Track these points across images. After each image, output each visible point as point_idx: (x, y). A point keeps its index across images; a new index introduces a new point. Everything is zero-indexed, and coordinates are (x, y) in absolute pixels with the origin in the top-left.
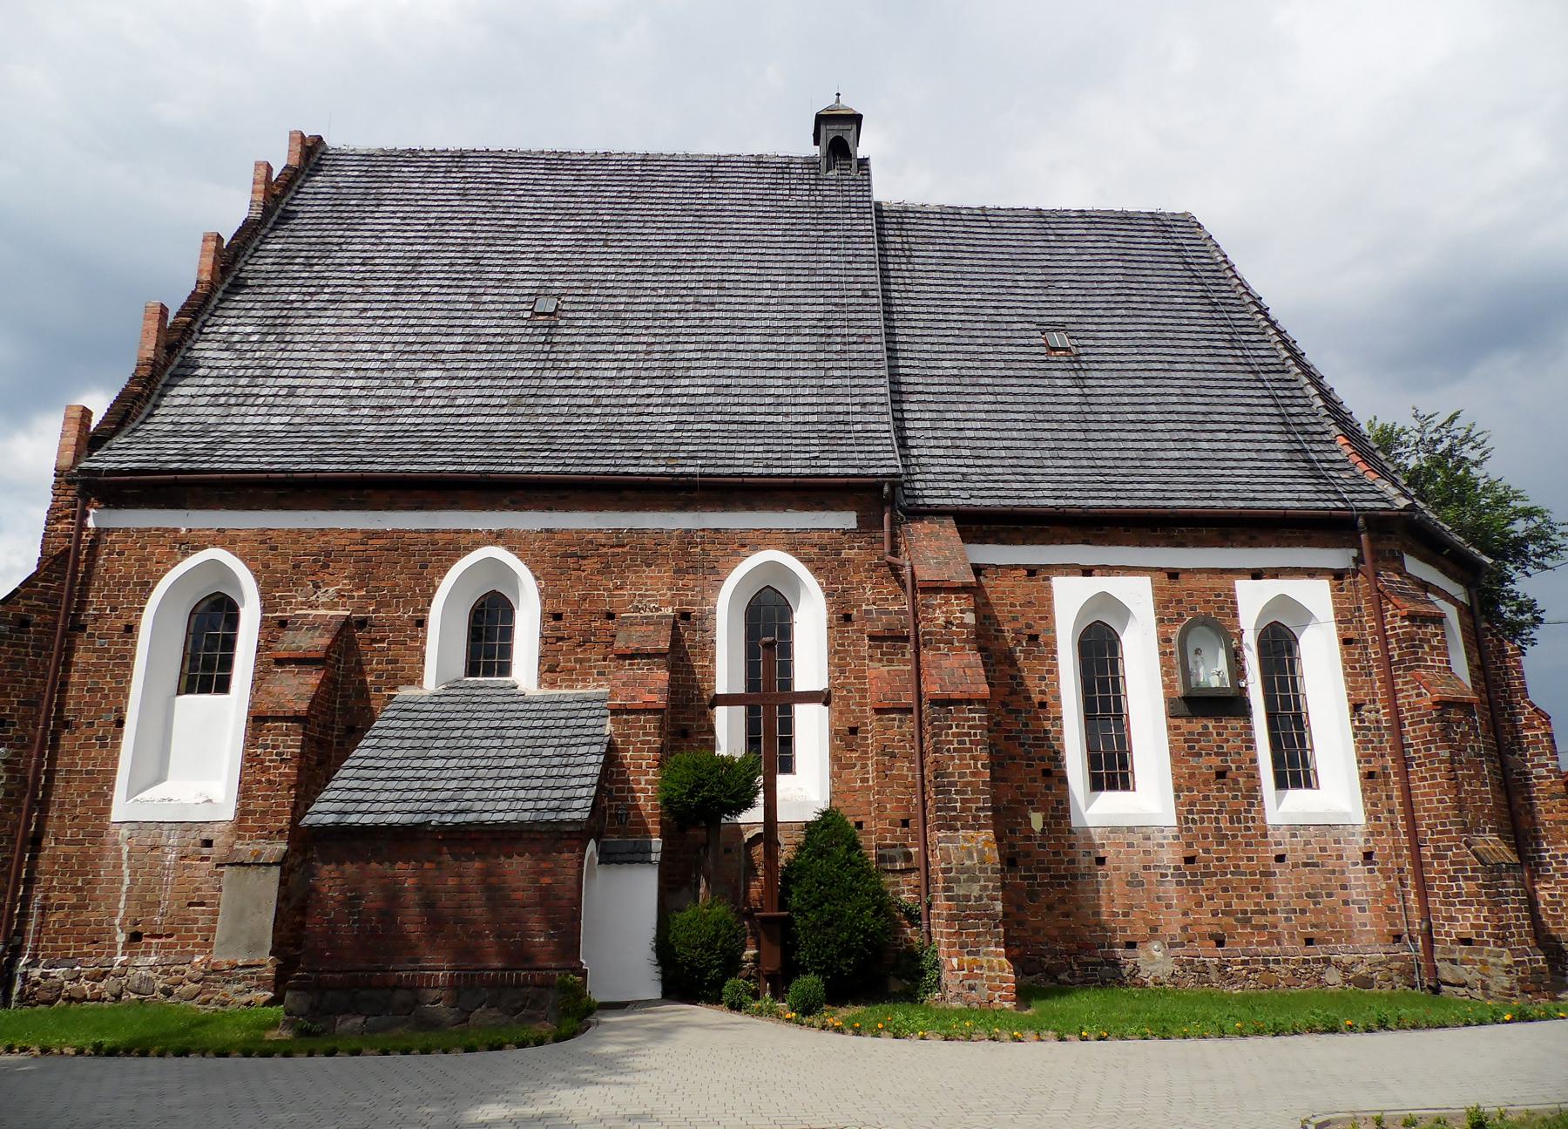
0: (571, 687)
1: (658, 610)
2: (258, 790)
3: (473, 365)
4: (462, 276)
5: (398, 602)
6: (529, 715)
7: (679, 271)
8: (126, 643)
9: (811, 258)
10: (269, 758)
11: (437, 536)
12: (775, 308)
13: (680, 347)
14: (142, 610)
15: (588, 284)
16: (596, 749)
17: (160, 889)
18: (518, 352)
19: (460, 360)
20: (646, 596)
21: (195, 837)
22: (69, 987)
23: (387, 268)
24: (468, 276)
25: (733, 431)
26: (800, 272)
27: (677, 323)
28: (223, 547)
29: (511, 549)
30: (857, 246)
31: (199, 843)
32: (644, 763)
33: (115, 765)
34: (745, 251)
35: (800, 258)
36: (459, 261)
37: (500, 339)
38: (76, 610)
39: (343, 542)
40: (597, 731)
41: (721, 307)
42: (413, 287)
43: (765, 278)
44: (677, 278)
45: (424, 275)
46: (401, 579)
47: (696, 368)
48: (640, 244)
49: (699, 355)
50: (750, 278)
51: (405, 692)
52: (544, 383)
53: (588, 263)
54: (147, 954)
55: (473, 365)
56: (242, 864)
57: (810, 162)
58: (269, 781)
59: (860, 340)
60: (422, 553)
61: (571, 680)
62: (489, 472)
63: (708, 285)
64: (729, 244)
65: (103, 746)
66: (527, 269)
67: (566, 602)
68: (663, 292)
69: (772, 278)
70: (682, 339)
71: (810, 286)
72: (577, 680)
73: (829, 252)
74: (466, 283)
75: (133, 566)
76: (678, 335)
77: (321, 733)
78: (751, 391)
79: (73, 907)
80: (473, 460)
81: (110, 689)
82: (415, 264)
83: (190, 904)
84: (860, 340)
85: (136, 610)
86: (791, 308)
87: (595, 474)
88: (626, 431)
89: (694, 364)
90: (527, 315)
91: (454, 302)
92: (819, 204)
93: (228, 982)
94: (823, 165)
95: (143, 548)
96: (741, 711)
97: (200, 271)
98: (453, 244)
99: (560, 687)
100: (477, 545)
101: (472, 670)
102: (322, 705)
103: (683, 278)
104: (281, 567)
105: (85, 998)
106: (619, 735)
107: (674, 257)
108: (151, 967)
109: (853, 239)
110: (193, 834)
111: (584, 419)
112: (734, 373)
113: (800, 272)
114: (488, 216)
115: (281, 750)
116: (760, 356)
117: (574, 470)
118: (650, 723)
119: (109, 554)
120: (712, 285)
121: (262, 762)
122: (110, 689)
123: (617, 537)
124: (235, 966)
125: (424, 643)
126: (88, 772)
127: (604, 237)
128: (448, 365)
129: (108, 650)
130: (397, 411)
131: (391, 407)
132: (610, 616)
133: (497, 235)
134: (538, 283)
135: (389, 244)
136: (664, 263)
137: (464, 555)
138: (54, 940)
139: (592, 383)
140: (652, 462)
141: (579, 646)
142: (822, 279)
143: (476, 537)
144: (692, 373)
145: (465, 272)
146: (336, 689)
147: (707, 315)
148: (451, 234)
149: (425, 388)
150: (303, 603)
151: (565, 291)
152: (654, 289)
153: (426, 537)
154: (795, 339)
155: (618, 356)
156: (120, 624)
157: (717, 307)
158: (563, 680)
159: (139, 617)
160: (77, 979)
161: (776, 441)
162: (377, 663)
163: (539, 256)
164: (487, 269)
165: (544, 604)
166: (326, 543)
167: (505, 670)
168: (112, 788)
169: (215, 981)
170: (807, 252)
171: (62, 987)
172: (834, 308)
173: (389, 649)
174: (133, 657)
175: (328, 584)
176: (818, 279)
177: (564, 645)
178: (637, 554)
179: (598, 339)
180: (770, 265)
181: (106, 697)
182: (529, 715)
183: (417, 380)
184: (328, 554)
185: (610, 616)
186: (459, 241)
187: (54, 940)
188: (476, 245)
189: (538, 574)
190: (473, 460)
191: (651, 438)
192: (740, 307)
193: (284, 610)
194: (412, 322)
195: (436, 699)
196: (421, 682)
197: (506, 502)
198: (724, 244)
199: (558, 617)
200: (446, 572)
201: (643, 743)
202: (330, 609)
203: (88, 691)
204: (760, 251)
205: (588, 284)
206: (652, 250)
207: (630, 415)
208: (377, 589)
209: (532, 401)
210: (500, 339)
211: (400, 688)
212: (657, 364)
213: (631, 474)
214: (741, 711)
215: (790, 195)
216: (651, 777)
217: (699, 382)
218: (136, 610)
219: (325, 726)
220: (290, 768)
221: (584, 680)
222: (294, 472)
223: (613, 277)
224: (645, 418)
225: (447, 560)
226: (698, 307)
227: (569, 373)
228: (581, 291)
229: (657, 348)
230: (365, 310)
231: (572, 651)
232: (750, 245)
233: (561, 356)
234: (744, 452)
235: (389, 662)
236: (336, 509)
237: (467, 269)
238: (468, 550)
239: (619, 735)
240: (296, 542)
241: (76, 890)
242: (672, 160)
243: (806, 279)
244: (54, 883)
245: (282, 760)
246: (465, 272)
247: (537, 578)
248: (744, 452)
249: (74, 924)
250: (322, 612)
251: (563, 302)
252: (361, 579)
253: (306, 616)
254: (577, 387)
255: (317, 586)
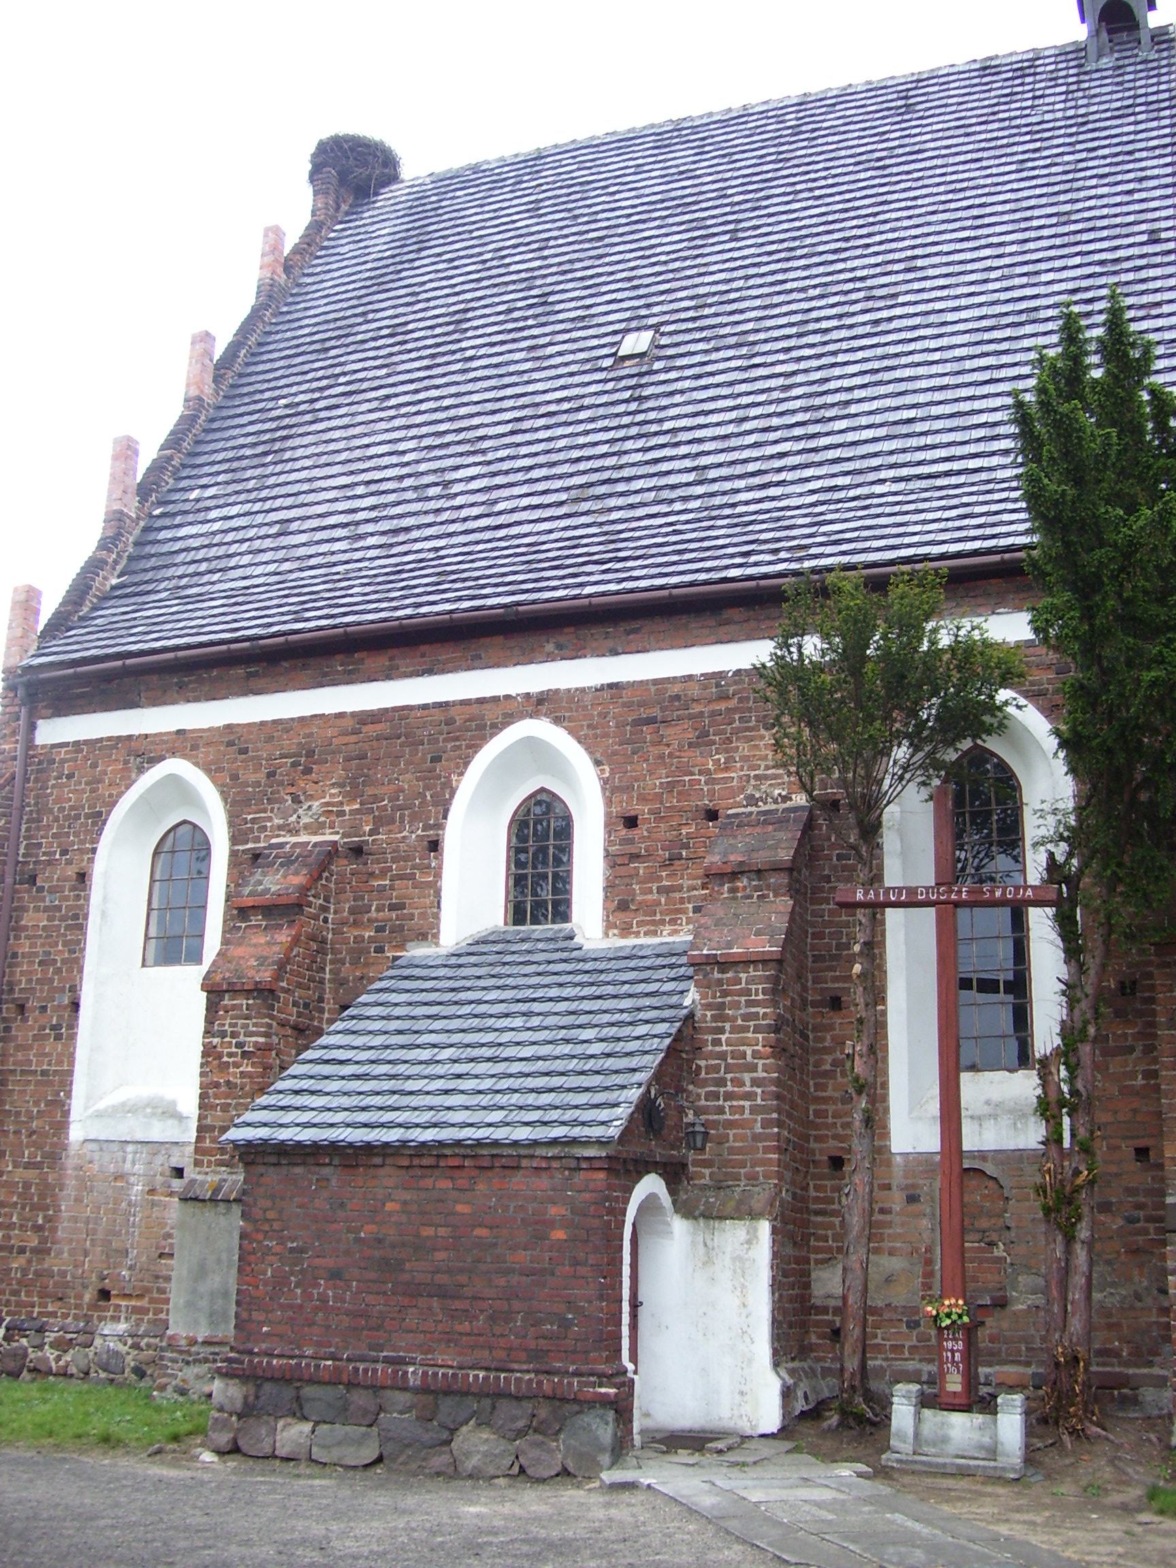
0: (655, 933)
1: (786, 799)
2: (216, 1096)
3: (524, 450)
4: (521, 324)
5: (402, 817)
6: (578, 978)
7: (843, 255)
8: (78, 897)
9: (1062, 198)
10: (228, 1048)
11: (452, 712)
12: (997, 285)
13: (837, 371)
14: (94, 851)
15: (700, 302)
16: (661, 1028)
17: (127, 1233)
18: (592, 420)
19: (507, 446)
20: (766, 777)
21: (162, 1163)
22: (32, 1356)
23: (422, 333)
24: (530, 322)
25: (912, 492)
26: (1042, 222)
27: (835, 335)
28: (184, 757)
29: (557, 721)
30: (1143, 164)
31: (168, 1173)
32: (749, 1053)
33: (72, 1063)
34: (953, 205)
35: (1044, 201)
36: (520, 304)
37: (566, 406)
38: (24, 855)
39: (330, 733)
40: (674, 1000)
41: (907, 298)
42: (454, 352)
43: (983, 242)
44: (840, 266)
45: (470, 334)
46: (407, 781)
47: (860, 401)
48: (786, 226)
49: (867, 379)
50: (959, 246)
51: (418, 951)
52: (625, 459)
53: (703, 270)
54: (116, 1319)
55: (524, 450)
56: (196, 1199)
57: (1075, 53)
58: (228, 1083)
59: (1141, 313)
60: (433, 741)
61: (653, 923)
62: (518, 604)
63: (889, 268)
64: (927, 201)
65: (58, 1037)
66: (614, 296)
67: (643, 799)
68: (817, 292)
69: (995, 240)
70: (841, 358)
71: (1058, 241)
72: (662, 922)
73: (1094, 182)
74: (526, 333)
75: (84, 791)
76: (834, 353)
77: (299, 1015)
78: (949, 423)
79: (35, 1251)
80: (501, 589)
81: (64, 961)
82: (459, 321)
83: (161, 1256)
84: (1141, 313)
85: (87, 851)
86: (1024, 280)
87: (676, 586)
88: (740, 515)
89: (858, 394)
90: (608, 362)
91: (714, 327)
92: (1082, 111)
93: (188, 1363)
94: (1092, 50)
95: (94, 766)
96: (928, 915)
97: (188, 385)
98: (514, 282)
99: (637, 934)
100: (509, 719)
101: (518, 914)
102: (299, 975)
103: (849, 264)
104: (252, 778)
105: (50, 1372)
106: (708, 1006)
107: (836, 236)
108: (120, 1338)
109: (1137, 155)
110: (160, 1159)
111: (678, 506)
112: (922, 398)
113: (1042, 222)
114: (565, 232)
115: (242, 1038)
116: (968, 364)
117: (643, 584)
118: (754, 982)
119: (57, 778)
120: (896, 267)
121: (220, 1056)
122: (64, 961)
123: (718, 685)
124: (192, 1342)
125: (438, 875)
126: (44, 1073)
127: (731, 227)
128: (490, 456)
129: (59, 908)
130: (415, 534)
131: (407, 530)
132: (712, 815)
133: (576, 256)
134: (627, 315)
135: (428, 300)
136: (821, 248)
137: (492, 736)
138: (15, 1293)
139: (695, 448)
140: (768, 558)
141: (664, 866)
142: (1080, 226)
143: (511, 707)
144: (853, 409)
145: (526, 318)
146: (322, 951)
147: (885, 314)
148: (513, 268)
149: (456, 495)
150: (280, 828)
151: (666, 318)
152: (803, 290)
153: (438, 715)
154: (1028, 329)
155: (738, 401)
156: (71, 872)
157: (901, 299)
158: (639, 924)
159: (91, 860)
160: (40, 1347)
161: (981, 498)
162: (378, 910)
163: (634, 273)
164: (558, 307)
165: (609, 802)
166: (307, 736)
167: (561, 911)
168: (69, 1095)
169: (174, 1361)
170: (1057, 188)
171: (26, 1355)
172: (1098, 269)
173: (392, 888)
174: (86, 917)
175: (311, 798)
176: (1073, 227)
177: (641, 868)
178: (750, 710)
179: (711, 380)
180: (1032, 202)
181: (58, 971)
182: (578, 978)
183: (447, 484)
184: (310, 754)
185: (712, 815)
186: (523, 275)
187: (15, 1293)
188: (545, 276)
189: (598, 756)
190: (501, 589)
191: (779, 519)
192: (939, 294)
193: (257, 840)
194: (446, 402)
195: (453, 961)
196: (436, 936)
197: (550, 647)
198: (920, 202)
199: (631, 822)
200: (467, 764)
201: (746, 1017)
202: (315, 833)
203: (40, 963)
204: (977, 201)
205: (700, 302)
206: (803, 232)
207: (750, 489)
208: (376, 799)
209: (603, 489)
210: (566, 406)
211: (409, 945)
212: (798, 404)
213: (733, 580)
214: (928, 915)
215: (1032, 107)
216: (761, 1074)
217: (864, 421)
218: (87, 851)
219: (306, 1006)
220: (253, 1064)
221: (673, 922)
222: (262, 637)
223: (741, 283)
224: (773, 492)
225: (469, 747)
226: (870, 304)
227: (662, 440)
228: (691, 314)
229: (800, 379)
230: (388, 397)
231: (652, 877)
232: (961, 195)
233: (652, 415)
234: (924, 522)
235: (393, 908)
236: (321, 685)
237: (530, 312)
238: (497, 728)
239: (708, 1006)
240: (270, 739)
241: (38, 1229)
242: (845, 96)
243: (1052, 231)
244: (14, 1219)
245: (244, 1053)
246: (526, 318)
247: (597, 763)
248: (924, 522)
249: (38, 1274)
250: (303, 838)
251: (663, 334)
252: (354, 787)
253: (282, 845)
254: (671, 458)
255: (296, 800)
